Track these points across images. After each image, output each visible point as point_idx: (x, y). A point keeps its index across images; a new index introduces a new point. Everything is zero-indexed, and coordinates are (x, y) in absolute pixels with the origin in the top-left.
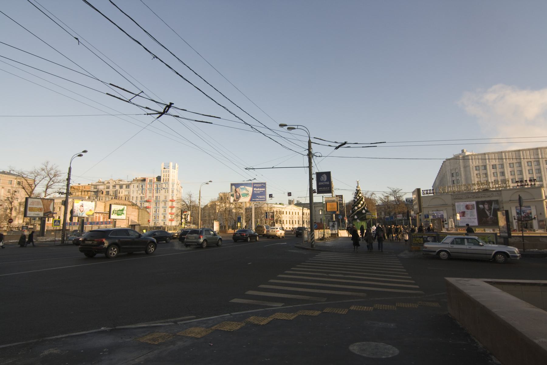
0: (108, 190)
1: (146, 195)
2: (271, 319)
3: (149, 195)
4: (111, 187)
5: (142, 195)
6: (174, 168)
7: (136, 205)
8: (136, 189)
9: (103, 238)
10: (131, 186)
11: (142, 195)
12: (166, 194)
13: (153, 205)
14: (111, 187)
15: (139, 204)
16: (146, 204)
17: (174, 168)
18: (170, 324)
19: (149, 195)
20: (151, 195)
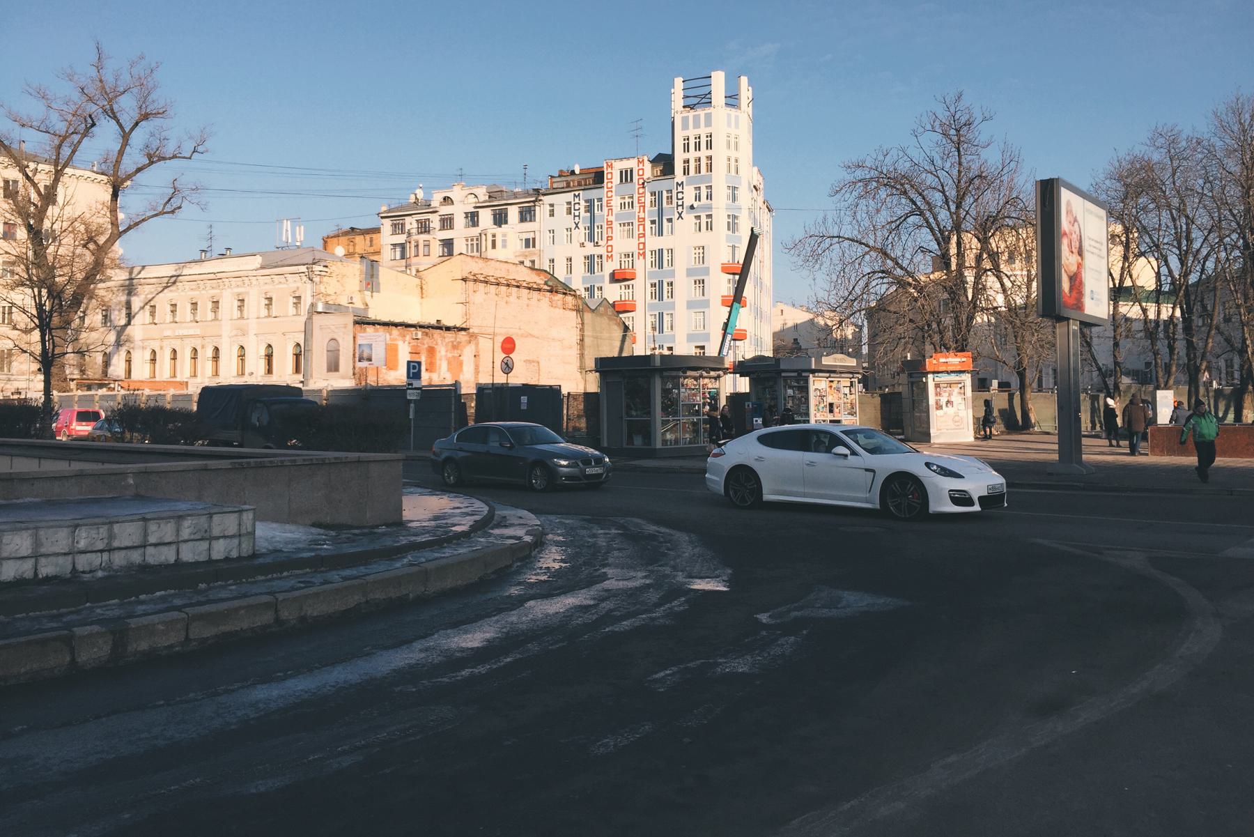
0: (447, 235)
1: (610, 249)
2: (290, 683)
3: (622, 243)
4: (460, 221)
5: (590, 249)
6: (732, 99)
7: (567, 290)
8: (563, 220)
9: (572, 567)
10: (541, 211)
11: (590, 249)
12: (704, 238)
13: (640, 291)
14: (460, 221)
15: (577, 284)
16: (613, 293)
17: (732, 99)
18: (954, 261)
19: (622, 243)
20: (632, 245)
